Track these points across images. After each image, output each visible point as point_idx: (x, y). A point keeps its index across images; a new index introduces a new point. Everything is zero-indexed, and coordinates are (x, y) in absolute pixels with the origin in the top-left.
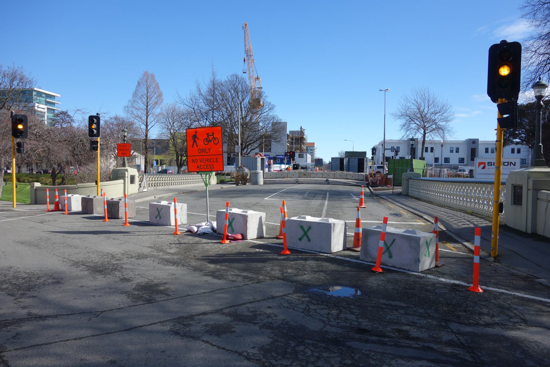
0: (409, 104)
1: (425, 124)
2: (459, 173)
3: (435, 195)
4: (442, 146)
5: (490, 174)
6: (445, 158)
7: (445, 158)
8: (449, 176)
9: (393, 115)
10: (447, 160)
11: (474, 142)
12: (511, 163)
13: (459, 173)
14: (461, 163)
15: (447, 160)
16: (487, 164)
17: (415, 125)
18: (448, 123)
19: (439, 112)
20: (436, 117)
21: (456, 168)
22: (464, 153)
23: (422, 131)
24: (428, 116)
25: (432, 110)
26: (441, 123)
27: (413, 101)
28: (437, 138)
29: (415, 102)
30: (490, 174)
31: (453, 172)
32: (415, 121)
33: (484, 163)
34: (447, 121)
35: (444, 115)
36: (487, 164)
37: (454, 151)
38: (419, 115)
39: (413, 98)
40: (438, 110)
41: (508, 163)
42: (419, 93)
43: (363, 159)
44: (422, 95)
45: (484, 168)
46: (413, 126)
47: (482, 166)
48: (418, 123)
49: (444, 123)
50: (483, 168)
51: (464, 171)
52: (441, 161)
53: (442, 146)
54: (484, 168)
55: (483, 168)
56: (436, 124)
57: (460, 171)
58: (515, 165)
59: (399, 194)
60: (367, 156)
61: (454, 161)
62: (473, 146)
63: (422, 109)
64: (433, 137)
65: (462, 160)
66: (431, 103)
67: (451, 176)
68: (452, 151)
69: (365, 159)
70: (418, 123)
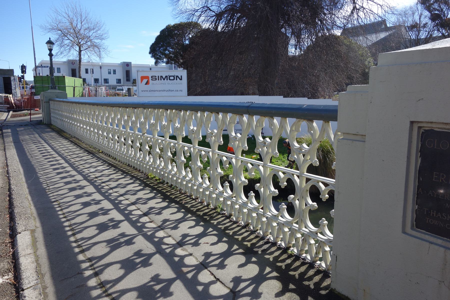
0: (60, 18)
1: (80, 41)
2: (117, 92)
3: (91, 131)
4: (101, 67)
5: (154, 91)
6: (104, 79)
7: (104, 79)
8: (108, 95)
9: (41, 27)
10: (106, 81)
11: (128, 65)
12: (177, 76)
13: (117, 92)
14: (119, 83)
15: (106, 81)
16: (150, 79)
17: (68, 41)
18: (103, 41)
19: (93, 29)
20: (91, 34)
21: (114, 88)
22: (120, 75)
23: (78, 49)
24: (82, 32)
25: (86, 26)
26: (96, 41)
27: (64, 15)
28: (95, 59)
29: (67, 16)
30: (154, 91)
31: (112, 91)
32: (68, 36)
33: (147, 77)
34: (102, 39)
35: (99, 32)
36: (150, 79)
37: (112, 72)
38: (72, 31)
39: (64, 11)
40: (92, 26)
41: (174, 76)
42: (70, 5)
43: (10, 78)
44: (73, 9)
45: (147, 83)
46: (67, 42)
47: (145, 81)
48: (71, 38)
49: (99, 41)
50: (146, 84)
51: (122, 90)
52: (101, 81)
53: (101, 67)
54: (147, 83)
55: (146, 84)
56: (91, 41)
57: (118, 90)
58: (181, 79)
59: (39, 123)
60: (15, 74)
61: (113, 81)
62: (128, 68)
63: (74, 24)
64: (90, 58)
65: (119, 81)
66: (83, 18)
67: (111, 95)
68: (110, 73)
69: (12, 78)
70: (71, 38)
